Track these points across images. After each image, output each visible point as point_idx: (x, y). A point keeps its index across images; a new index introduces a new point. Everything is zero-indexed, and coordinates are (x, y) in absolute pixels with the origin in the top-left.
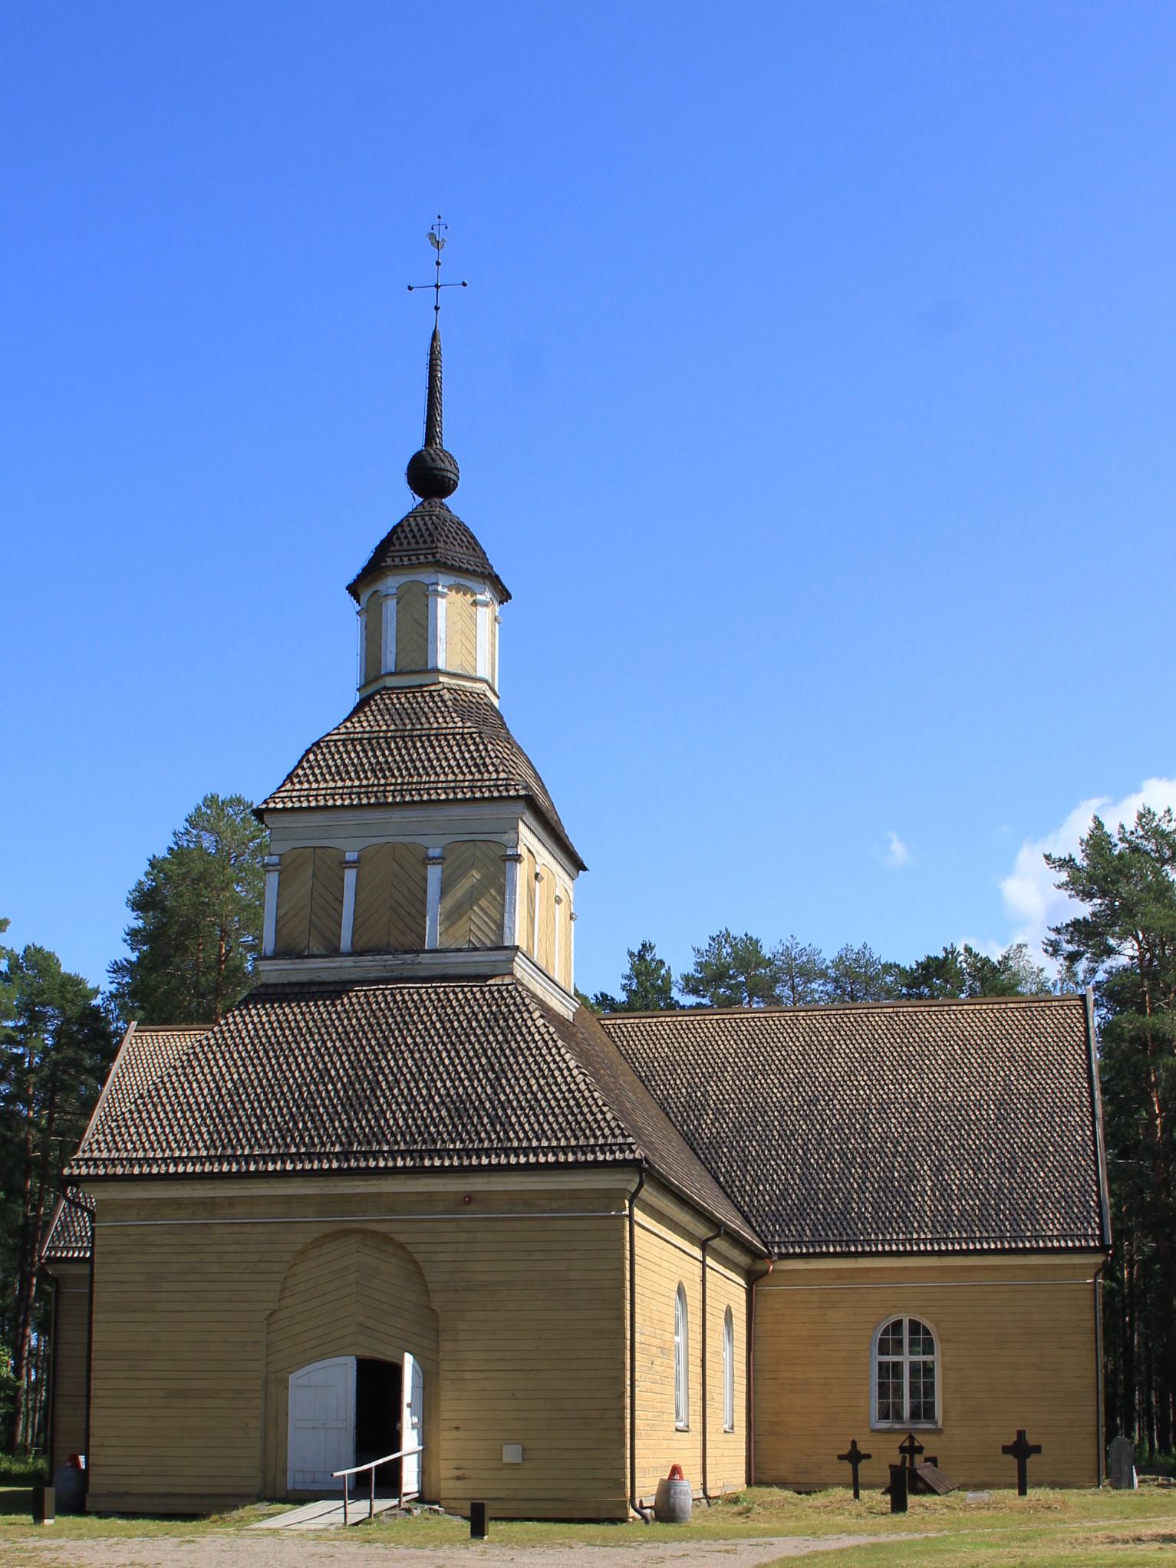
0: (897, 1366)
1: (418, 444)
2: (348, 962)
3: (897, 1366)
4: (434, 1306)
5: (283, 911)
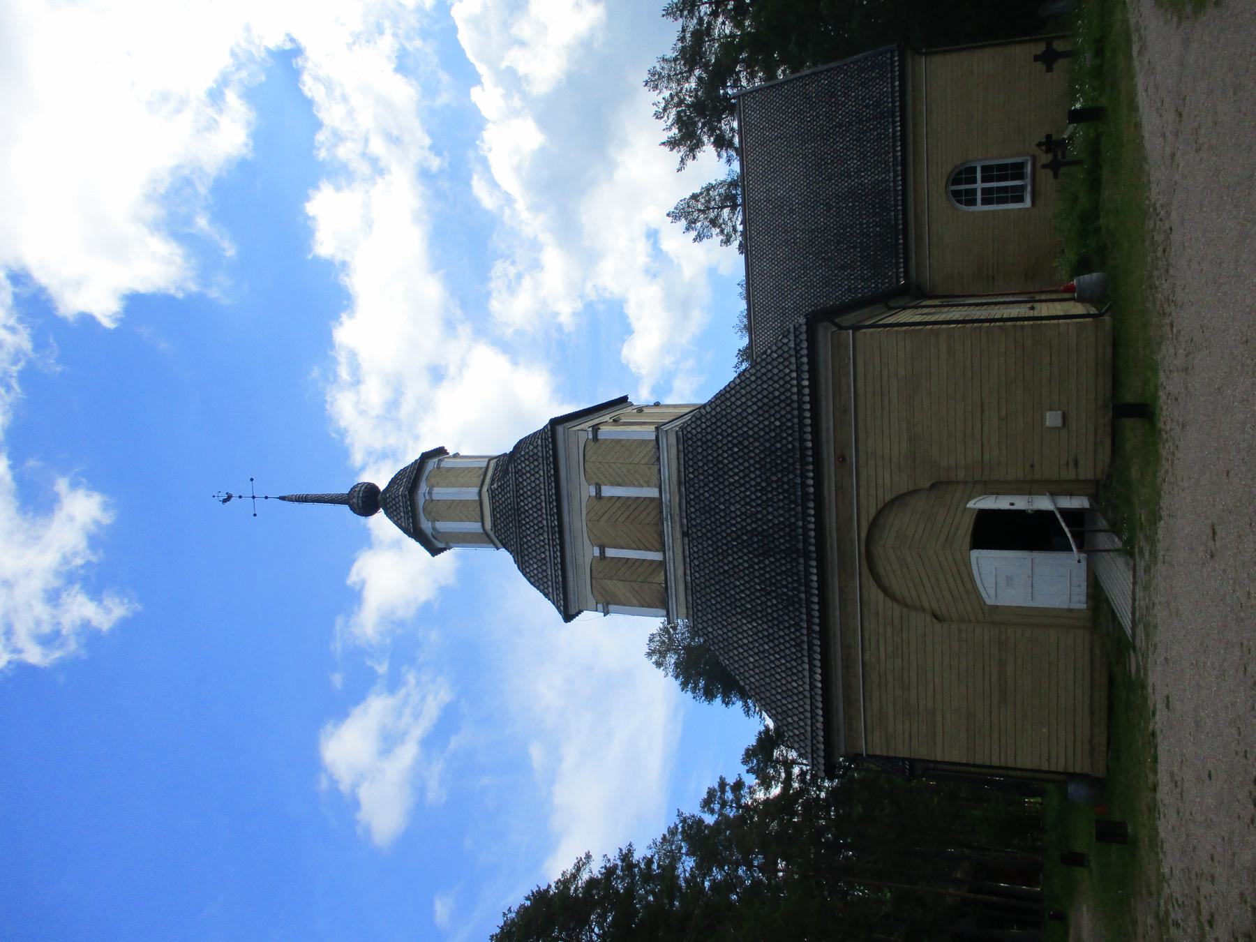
0: (984, 191)
1: (346, 508)
2: (669, 554)
3: (984, 191)
4: (927, 485)
5: (635, 602)
